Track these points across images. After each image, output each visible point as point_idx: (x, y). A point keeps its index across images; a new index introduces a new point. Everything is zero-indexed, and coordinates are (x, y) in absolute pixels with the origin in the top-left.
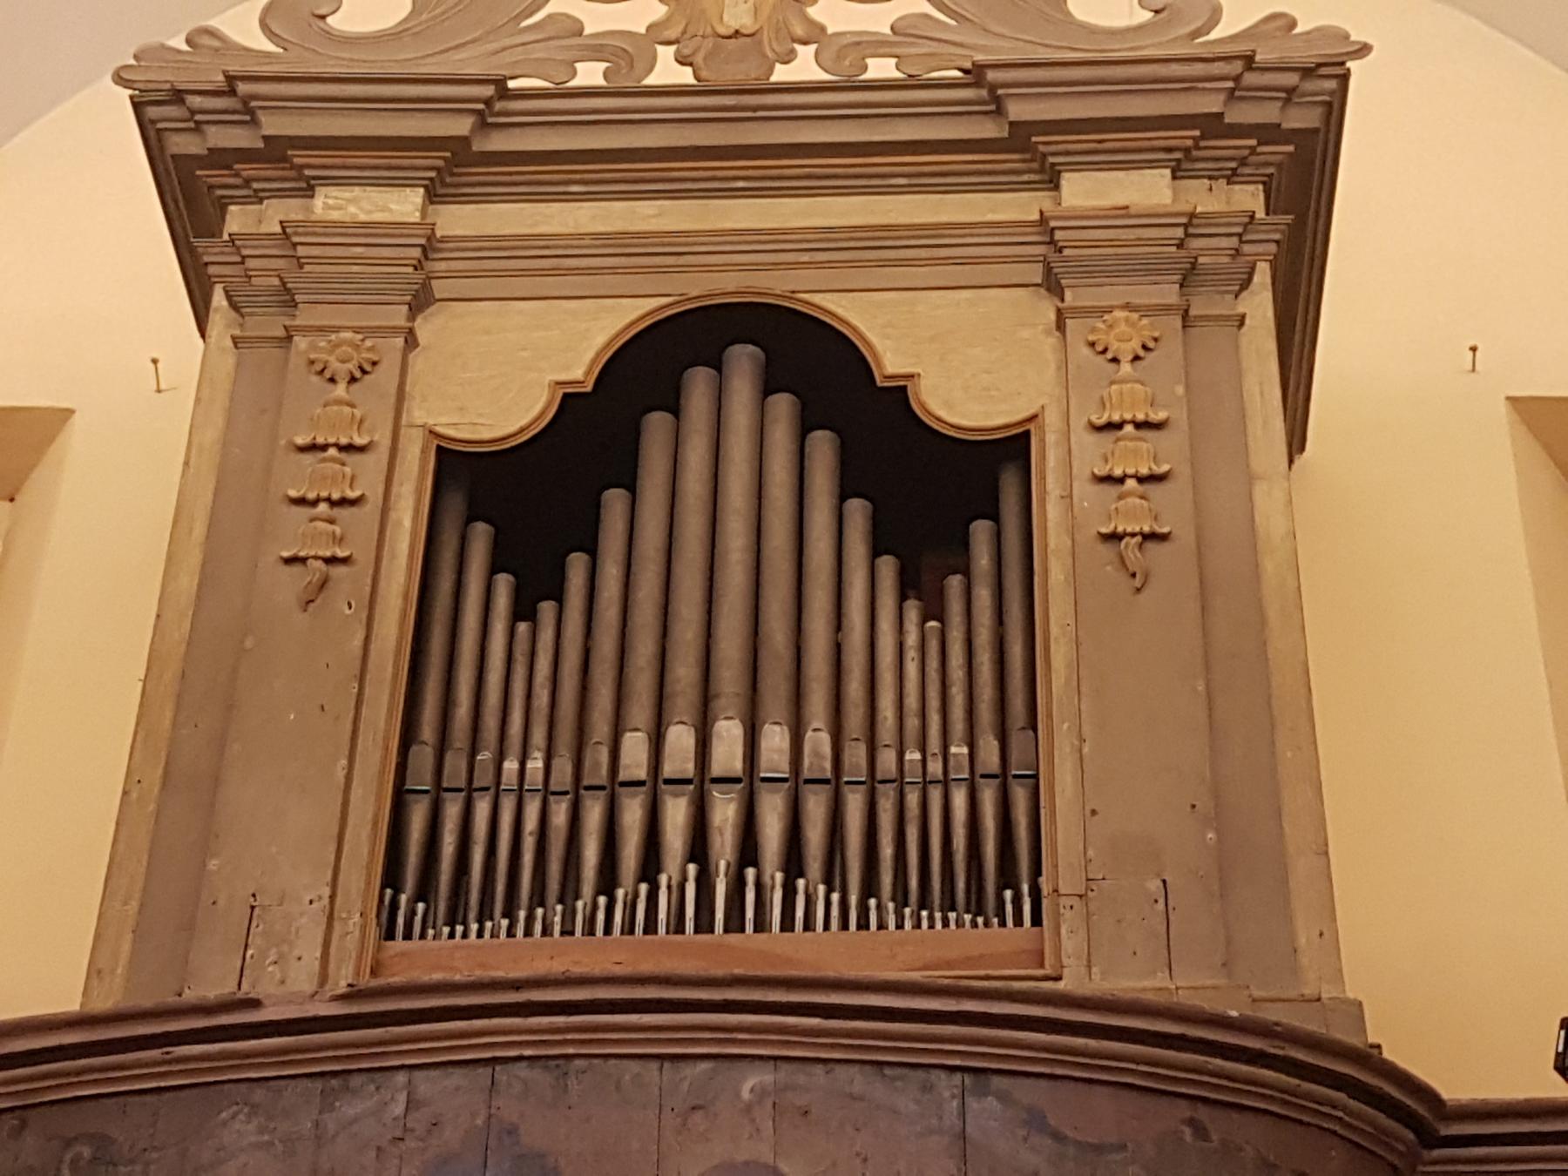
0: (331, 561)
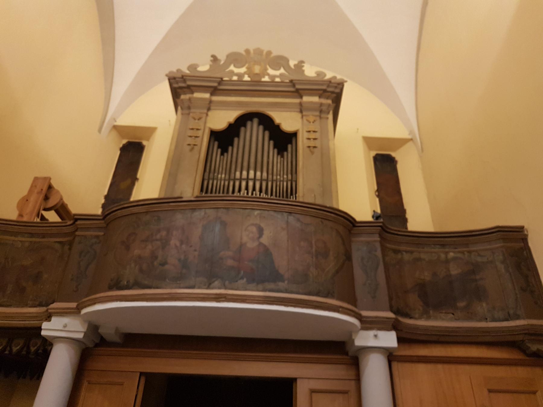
0: (195, 145)
